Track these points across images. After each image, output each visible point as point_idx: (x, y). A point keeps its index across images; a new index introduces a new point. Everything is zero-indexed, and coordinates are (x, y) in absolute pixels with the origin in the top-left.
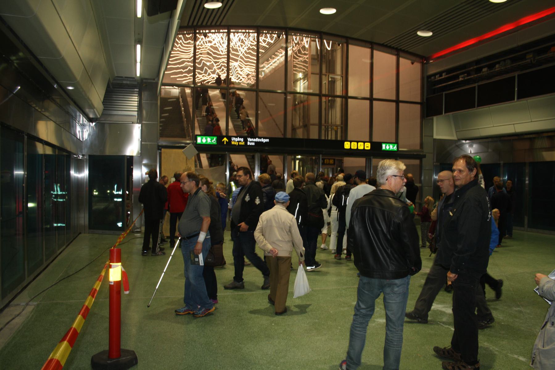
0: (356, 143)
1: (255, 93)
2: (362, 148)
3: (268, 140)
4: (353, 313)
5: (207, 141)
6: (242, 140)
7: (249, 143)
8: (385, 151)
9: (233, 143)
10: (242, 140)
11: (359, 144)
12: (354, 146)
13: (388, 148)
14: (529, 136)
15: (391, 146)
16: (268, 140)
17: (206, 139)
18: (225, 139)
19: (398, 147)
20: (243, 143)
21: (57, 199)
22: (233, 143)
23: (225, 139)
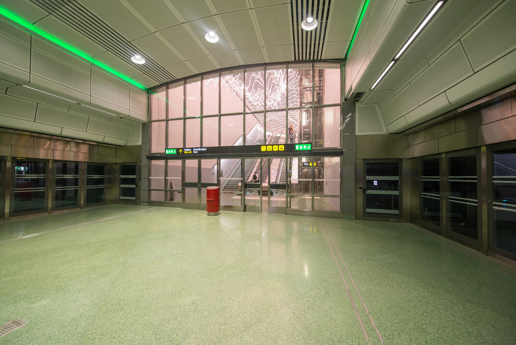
0: (271, 147)
1: (222, 117)
2: (277, 150)
3: (206, 149)
4: (200, 219)
5: (303, 148)
6: (190, 150)
7: (194, 152)
8: (298, 151)
9: (185, 152)
10: (190, 150)
11: (274, 146)
12: (269, 149)
13: (170, 152)
14: (509, 90)
15: (172, 151)
16: (206, 149)
17: (303, 146)
18: (181, 150)
19: (312, 147)
20: (191, 152)
21: (314, 181)
22: (185, 152)
23: (181, 150)
